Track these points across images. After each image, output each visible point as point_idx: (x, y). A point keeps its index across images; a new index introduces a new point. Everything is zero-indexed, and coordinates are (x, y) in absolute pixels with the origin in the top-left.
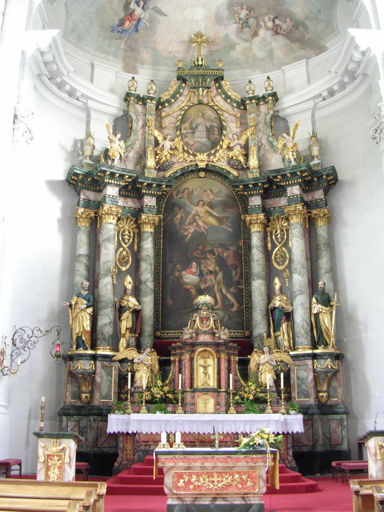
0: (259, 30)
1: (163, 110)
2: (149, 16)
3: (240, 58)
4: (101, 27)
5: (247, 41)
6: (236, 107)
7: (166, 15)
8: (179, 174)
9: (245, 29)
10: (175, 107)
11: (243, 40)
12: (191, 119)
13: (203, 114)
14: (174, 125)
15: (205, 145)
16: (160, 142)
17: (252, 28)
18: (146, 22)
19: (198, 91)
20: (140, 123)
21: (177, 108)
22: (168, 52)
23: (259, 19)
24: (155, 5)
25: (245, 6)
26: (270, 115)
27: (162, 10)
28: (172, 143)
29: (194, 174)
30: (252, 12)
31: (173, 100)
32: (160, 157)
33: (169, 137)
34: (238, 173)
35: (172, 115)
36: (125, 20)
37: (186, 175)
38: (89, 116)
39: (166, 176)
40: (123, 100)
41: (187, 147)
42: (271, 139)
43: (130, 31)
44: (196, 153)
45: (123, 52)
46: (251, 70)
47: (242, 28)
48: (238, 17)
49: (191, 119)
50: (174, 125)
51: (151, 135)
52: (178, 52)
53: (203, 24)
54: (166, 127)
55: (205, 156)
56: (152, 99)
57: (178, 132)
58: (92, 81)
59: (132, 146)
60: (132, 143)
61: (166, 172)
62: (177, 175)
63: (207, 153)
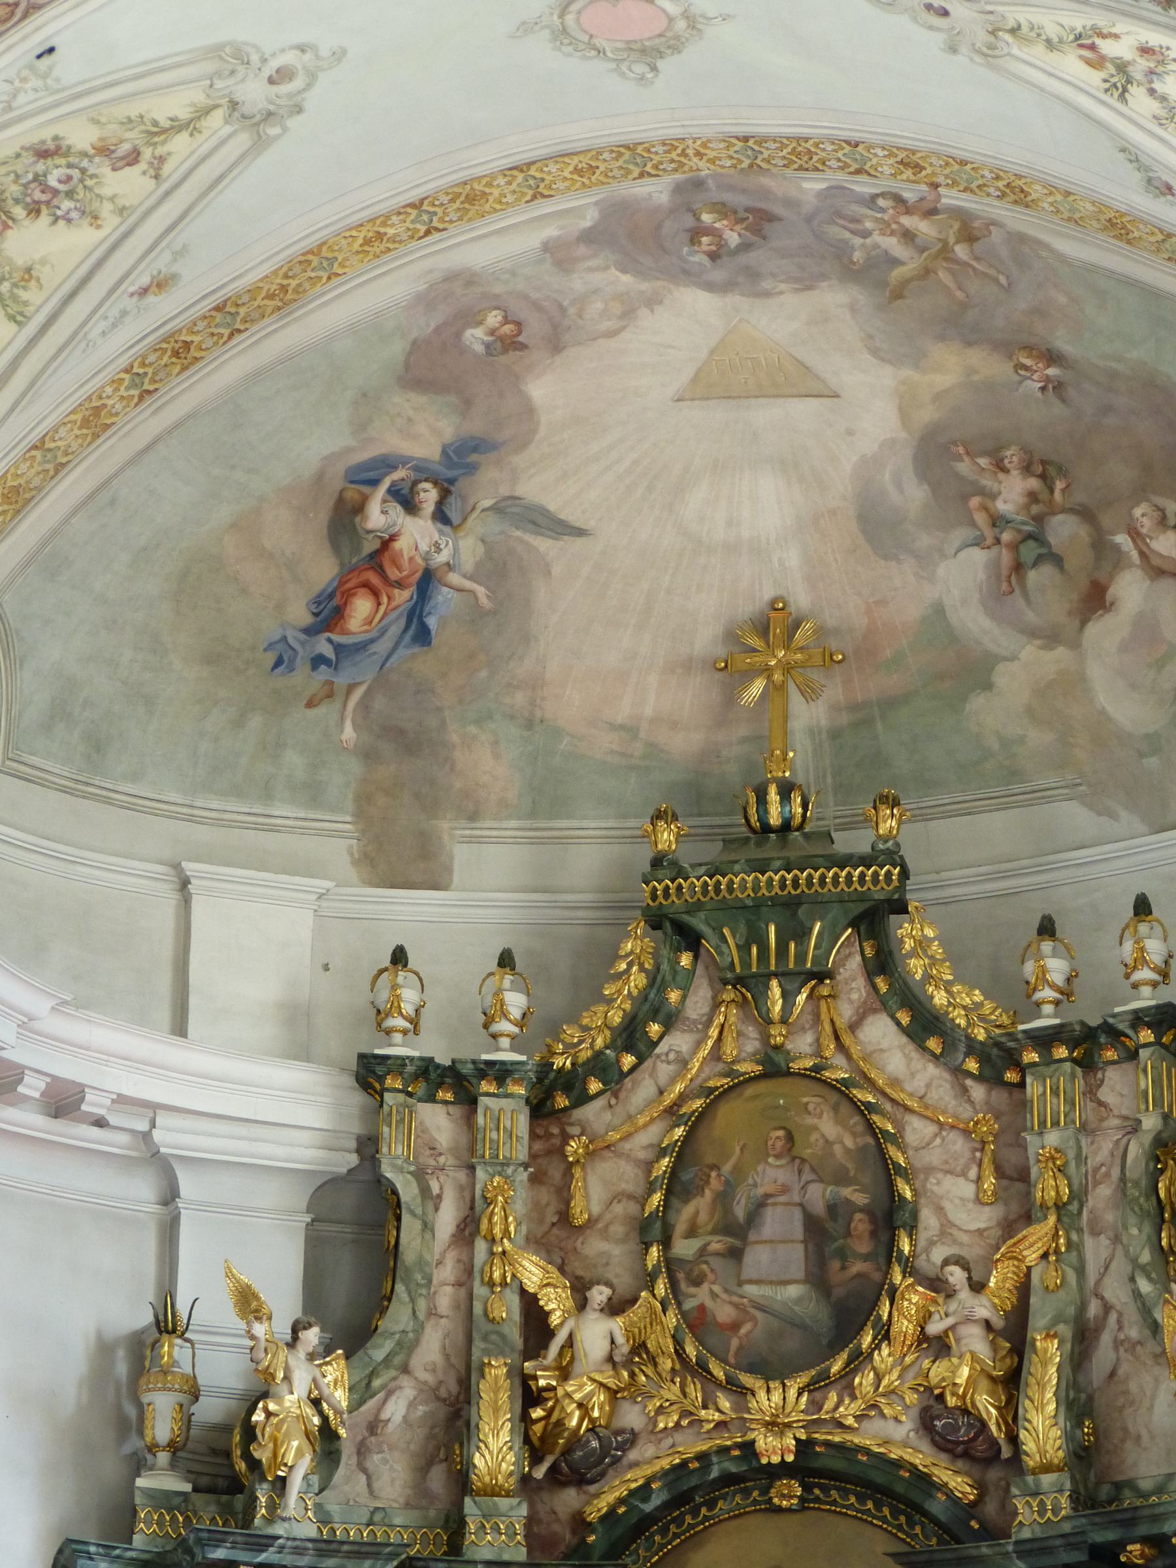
0: (1111, 577)
1: (579, 1113)
2: (481, 549)
3: (1022, 740)
4: (210, 659)
5: (1051, 637)
6: (980, 1078)
7: (580, 532)
8: (656, 1501)
9: (1032, 576)
10: (642, 1091)
11: (1032, 633)
12: (727, 1168)
13: (790, 1138)
14: (632, 1208)
15: (799, 1325)
16: (555, 1320)
17: (1071, 563)
18: (468, 584)
19: (761, 996)
20: (447, 1218)
21: (649, 1104)
22: (613, 727)
23: (1106, 520)
24: (504, 491)
25: (1012, 456)
26: (1147, 1139)
27: (552, 507)
28: (617, 1325)
29: (747, 1493)
30: (1059, 485)
31: (628, 1060)
32: (550, 1412)
33: (599, 1295)
34: (981, 1486)
35: (627, 1146)
36: (348, 595)
37: (698, 1499)
38: (170, 1196)
39: (593, 1517)
40: (350, 1081)
41: (700, 1340)
42: (1145, 1286)
43: (382, 647)
44: (746, 1379)
45: (355, 767)
46: (1091, 807)
47: (1018, 568)
48: (986, 509)
49: (727, 1168)
50: (632, 1208)
51: (504, 1284)
52: (674, 725)
53: (793, 558)
54: (591, 1222)
55: (792, 1393)
56: (501, 1073)
57: (654, 1251)
58: (180, 1029)
59: (397, 1360)
60: (399, 1343)
61: (592, 1489)
62: (648, 1508)
63: (803, 1379)
